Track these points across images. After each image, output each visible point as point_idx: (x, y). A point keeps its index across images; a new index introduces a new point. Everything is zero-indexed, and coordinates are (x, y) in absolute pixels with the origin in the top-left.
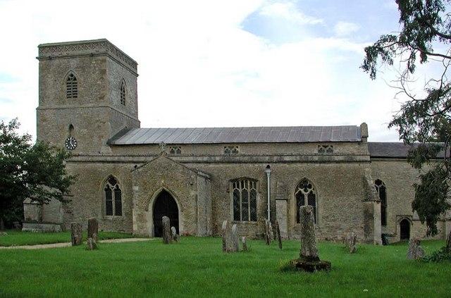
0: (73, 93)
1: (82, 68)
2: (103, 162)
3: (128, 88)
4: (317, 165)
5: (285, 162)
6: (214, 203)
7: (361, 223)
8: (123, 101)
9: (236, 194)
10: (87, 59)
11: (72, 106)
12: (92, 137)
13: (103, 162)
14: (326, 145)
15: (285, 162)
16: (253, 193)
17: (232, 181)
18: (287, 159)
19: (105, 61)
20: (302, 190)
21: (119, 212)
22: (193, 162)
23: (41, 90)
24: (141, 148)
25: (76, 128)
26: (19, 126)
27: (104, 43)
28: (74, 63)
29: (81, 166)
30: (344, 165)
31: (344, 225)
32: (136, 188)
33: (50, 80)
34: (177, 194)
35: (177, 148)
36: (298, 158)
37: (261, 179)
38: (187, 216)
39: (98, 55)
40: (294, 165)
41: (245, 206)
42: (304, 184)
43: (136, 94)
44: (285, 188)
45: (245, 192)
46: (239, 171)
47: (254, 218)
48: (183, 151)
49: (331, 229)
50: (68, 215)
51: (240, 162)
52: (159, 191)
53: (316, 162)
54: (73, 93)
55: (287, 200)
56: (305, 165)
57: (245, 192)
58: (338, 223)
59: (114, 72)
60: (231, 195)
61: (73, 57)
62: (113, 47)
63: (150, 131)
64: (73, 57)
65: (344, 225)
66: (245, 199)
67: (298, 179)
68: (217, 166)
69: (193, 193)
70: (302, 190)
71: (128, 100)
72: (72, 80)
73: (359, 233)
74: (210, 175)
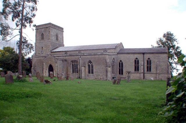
0: (43, 38)
1: (45, 31)
2: (42, 57)
3: (59, 36)
4: (93, 56)
5: (85, 55)
6: (67, 68)
7: (105, 74)
8: (57, 39)
9: (73, 65)
10: (46, 28)
11: (42, 42)
12: (47, 50)
13: (42, 57)
14: (105, 50)
15: (85, 55)
16: (77, 65)
17: (71, 61)
18: (85, 54)
19: (50, 29)
20: (89, 64)
21: (92, 73)
22: (62, 56)
23: (36, 38)
24: (57, 53)
25: (43, 48)
26: (152, 45)
27: (50, 24)
28: (43, 30)
29: (37, 58)
30: (100, 56)
31: (101, 74)
32: (44, 64)
33: (38, 35)
34: (53, 65)
35: (80, 52)
36: (88, 54)
37: (78, 61)
38: (55, 72)
39: (48, 27)
40: (87, 56)
41: (75, 69)
42: (90, 62)
43: (63, 37)
44: (84, 63)
45: (75, 64)
46: (73, 58)
47: (77, 72)
48: (108, 51)
49: (97, 75)
50: (35, 72)
51: (73, 56)
52: (49, 64)
53: (93, 55)
54: (43, 38)
55: (85, 67)
56: (90, 56)
57: (75, 64)
58: (99, 74)
59: (53, 32)
60: (72, 65)
61: (43, 28)
62: (53, 25)
63: (68, 47)
64: (43, 28)
65: (101, 74)
66: (75, 67)
67: (88, 60)
68: (68, 57)
69: (56, 65)
70: (89, 64)
71: (59, 39)
72: (42, 35)
73: (105, 77)
74: (65, 60)
